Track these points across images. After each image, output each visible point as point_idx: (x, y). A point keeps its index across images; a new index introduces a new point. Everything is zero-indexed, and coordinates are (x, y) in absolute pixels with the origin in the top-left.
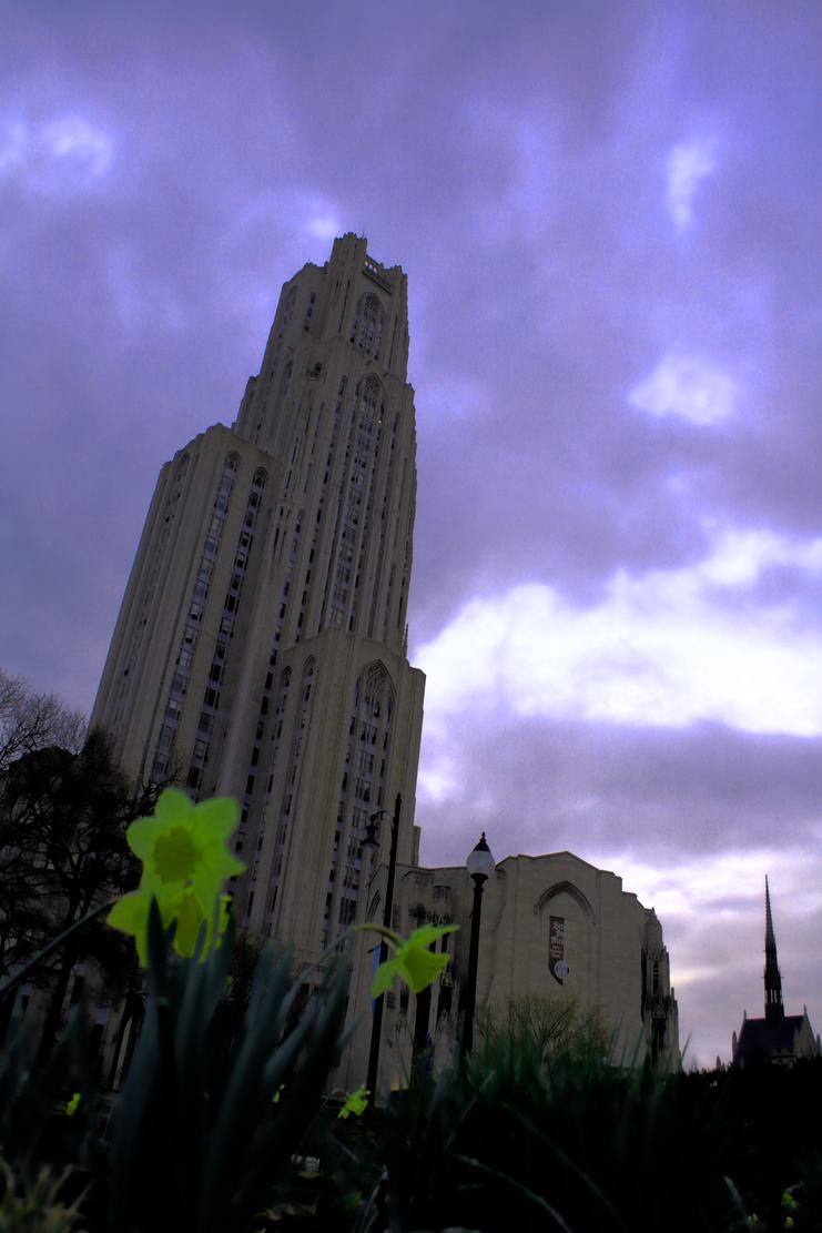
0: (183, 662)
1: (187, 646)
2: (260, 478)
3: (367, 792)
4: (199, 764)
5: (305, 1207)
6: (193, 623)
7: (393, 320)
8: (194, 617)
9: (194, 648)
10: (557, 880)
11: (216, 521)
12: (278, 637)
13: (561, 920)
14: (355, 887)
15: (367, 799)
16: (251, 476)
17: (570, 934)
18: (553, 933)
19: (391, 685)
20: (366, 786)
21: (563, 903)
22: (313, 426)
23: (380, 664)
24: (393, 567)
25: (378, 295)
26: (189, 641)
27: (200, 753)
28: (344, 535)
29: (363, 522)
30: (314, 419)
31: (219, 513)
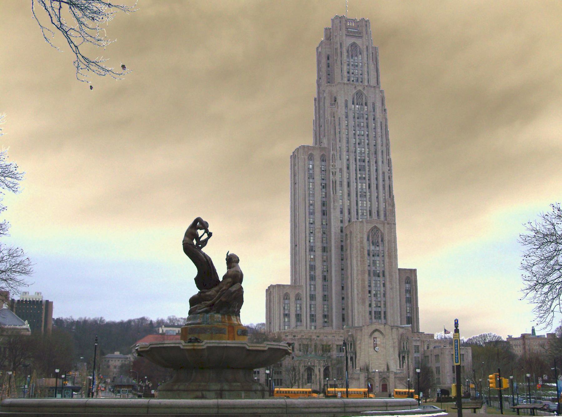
0: (312, 241)
1: (312, 235)
2: (323, 159)
3: (379, 273)
4: (325, 274)
5: (131, 379)
6: (312, 226)
7: (365, 50)
8: (312, 223)
9: (314, 235)
10: (374, 329)
11: (311, 184)
12: (342, 221)
13: (376, 338)
14: (380, 307)
15: (379, 276)
16: (371, 24)
17: (378, 341)
18: (374, 341)
19: (381, 232)
20: (378, 271)
21: (376, 334)
22: (337, 130)
23: (375, 227)
24: (384, 173)
25: (355, 41)
26: (312, 233)
27: (325, 270)
28: (360, 170)
29: (367, 161)
30: (337, 127)
31: (311, 180)
